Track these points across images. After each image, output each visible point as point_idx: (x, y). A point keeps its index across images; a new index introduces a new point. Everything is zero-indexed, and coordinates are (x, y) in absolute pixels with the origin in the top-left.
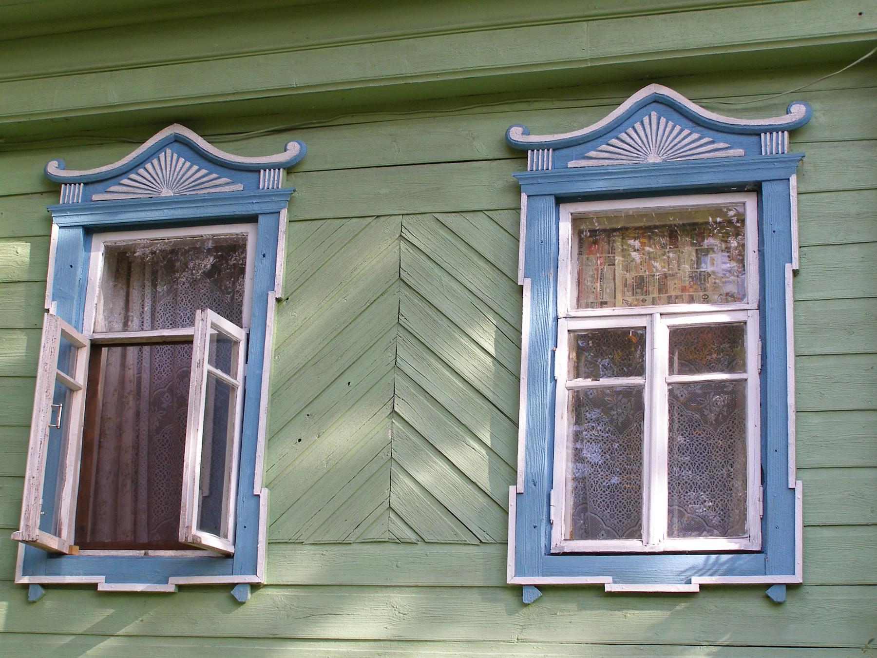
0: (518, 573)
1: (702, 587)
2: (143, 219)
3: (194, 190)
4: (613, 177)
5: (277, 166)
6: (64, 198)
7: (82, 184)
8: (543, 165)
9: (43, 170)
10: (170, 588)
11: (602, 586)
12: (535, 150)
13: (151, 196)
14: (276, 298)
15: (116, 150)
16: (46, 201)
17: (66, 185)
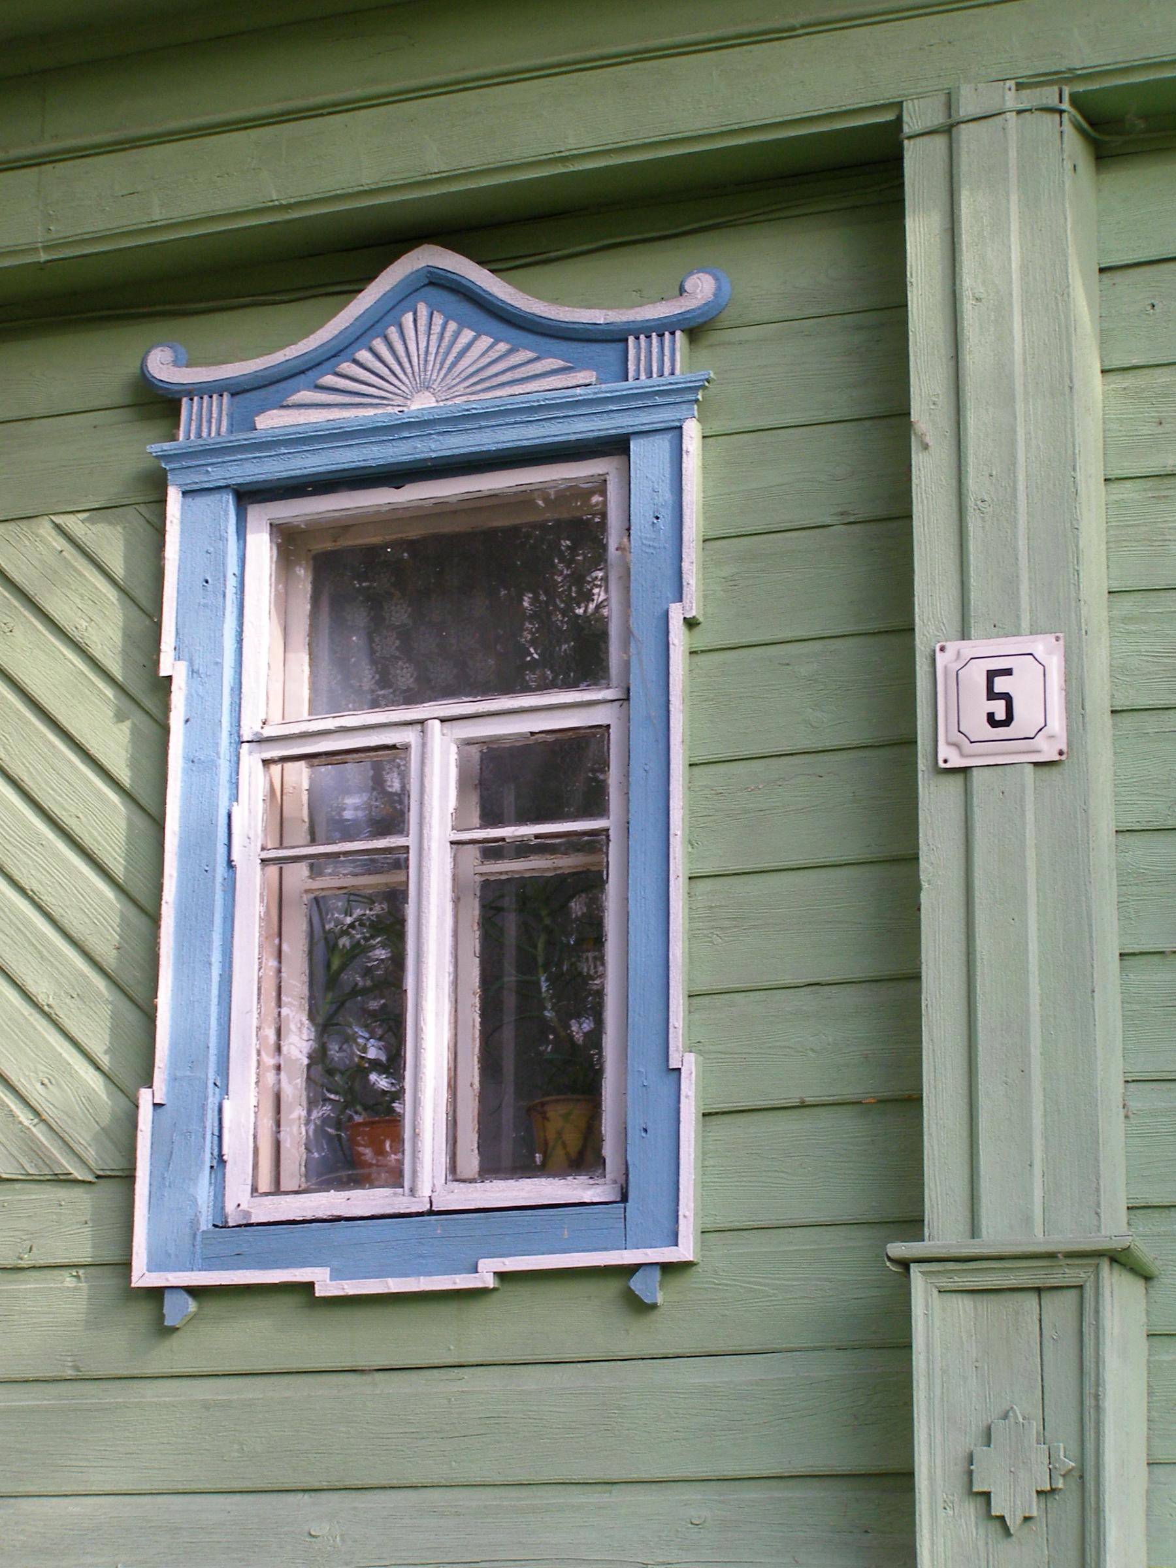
0: (154, 1265)
1: (501, 1276)
2: (457, 452)
4: (600, 409)
5: (662, 328)
9: (138, 364)
11: (311, 1285)
12: (667, 333)
14: (685, 618)
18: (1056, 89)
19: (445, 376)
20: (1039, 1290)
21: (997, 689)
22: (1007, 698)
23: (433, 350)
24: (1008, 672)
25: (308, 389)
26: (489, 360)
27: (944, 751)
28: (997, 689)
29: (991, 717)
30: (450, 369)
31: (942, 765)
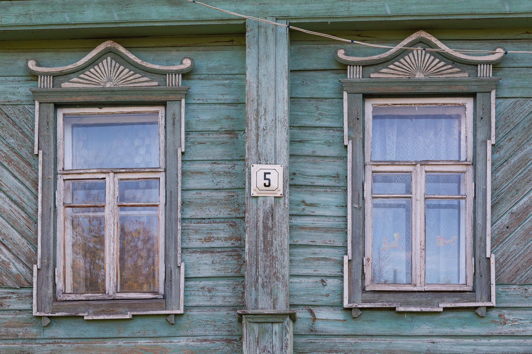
3: (437, 75)
5: (176, 72)
6: (350, 75)
7: (361, 66)
8: (486, 75)
10: (128, 317)
13: (409, 77)
15: (67, 55)
16: (339, 77)
17: (350, 66)
18: (286, 21)
19: (116, 78)
20: (272, 323)
21: (267, 177)
22: (269, 180)
23: (112, 70)
24: (269, 173)
25: (76, 77)
26: (128, 75)
27: (252, 192)
28: (267, 177)
29: (265, 184)
30: (117, 77)
31: (252, 195)
